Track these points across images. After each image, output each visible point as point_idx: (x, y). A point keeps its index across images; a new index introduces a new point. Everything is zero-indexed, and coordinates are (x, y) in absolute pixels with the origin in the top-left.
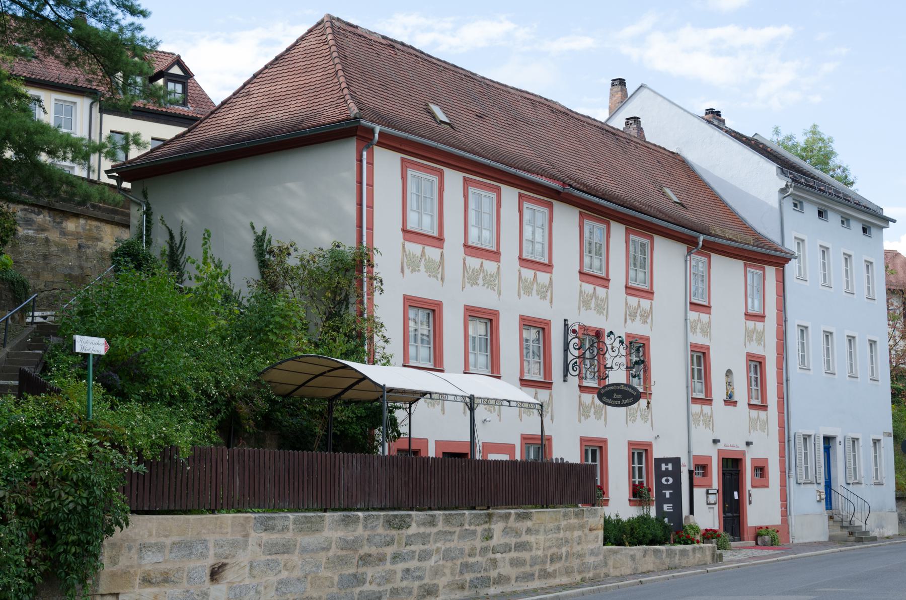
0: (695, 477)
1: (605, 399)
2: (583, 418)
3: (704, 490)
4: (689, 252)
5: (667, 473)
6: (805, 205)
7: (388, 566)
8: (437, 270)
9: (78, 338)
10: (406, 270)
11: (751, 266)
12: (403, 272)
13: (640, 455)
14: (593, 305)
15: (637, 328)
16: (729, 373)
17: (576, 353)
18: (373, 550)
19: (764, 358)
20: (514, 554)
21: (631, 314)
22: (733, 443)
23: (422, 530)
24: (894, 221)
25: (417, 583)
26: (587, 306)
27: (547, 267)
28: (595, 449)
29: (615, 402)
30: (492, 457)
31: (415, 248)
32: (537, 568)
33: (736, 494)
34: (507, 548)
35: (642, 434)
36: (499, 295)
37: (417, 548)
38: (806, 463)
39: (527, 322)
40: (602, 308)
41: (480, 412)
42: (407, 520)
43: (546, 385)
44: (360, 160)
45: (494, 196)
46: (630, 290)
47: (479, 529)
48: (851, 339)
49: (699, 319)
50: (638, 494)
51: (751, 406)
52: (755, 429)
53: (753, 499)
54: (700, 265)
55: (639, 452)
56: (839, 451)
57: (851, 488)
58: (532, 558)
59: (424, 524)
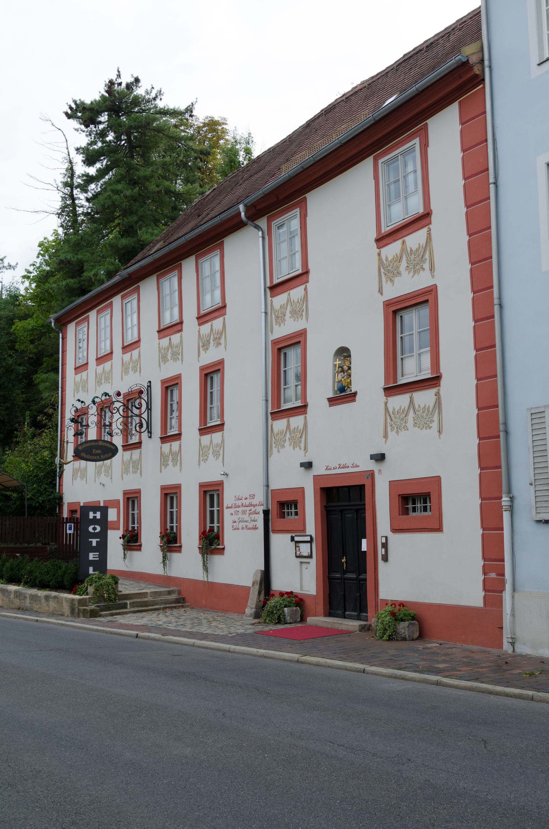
2: (163, 467)
5: (95, 521)
14: (169, 356)
16: (343, 353)
29: (95, 458)
36: (112, 385)
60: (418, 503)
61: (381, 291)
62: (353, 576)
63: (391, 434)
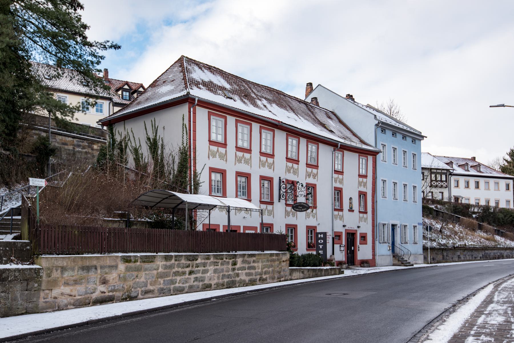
0: (335, 240)
1: (295, 208)
4: (334, 150)
5: (321, 238)
6: (387, 131)
7: (187, 276)
8: (223, 157)
9: (30, 179)
10: (211, 157)
11: (362, 156)
12: (209, 157)
13: (311, 231)
14: (292, 171)
15: (311, 181)
16: (351, 199)
17: (284, 190)
18: (180, 270)
19: (366, 193)
20: (247, 271)
21: (308, 175)
22: (352, 226)
23: (203, 261)
24: (426, 137)
25: (201, 283)
26: (289, 172)
27: (272, 156)
28: (292, 228)
30: (247, 232)
31: (214, 148)
32: (258, 277)
33: (353, 248)
34: (243, 269)
35: (312, 222)
37: (201, 268)
38: (384, 235)
39: (263, 178)
40: (296, 172)
41: (232, 212)
42: (196, 257)
43: (271, 203)
44: (190, 112)
45: (249, 127)
46: (308, 165)
47: (231, 261)
48: (405, 186)
50: (309, 246)
51: (360, 212)
52: (362, 221)
54: (339, 155)
55: (311, 230)
56: (398, 231)
57: (403, 245)
58: (256, 272)
59: (204, 259)
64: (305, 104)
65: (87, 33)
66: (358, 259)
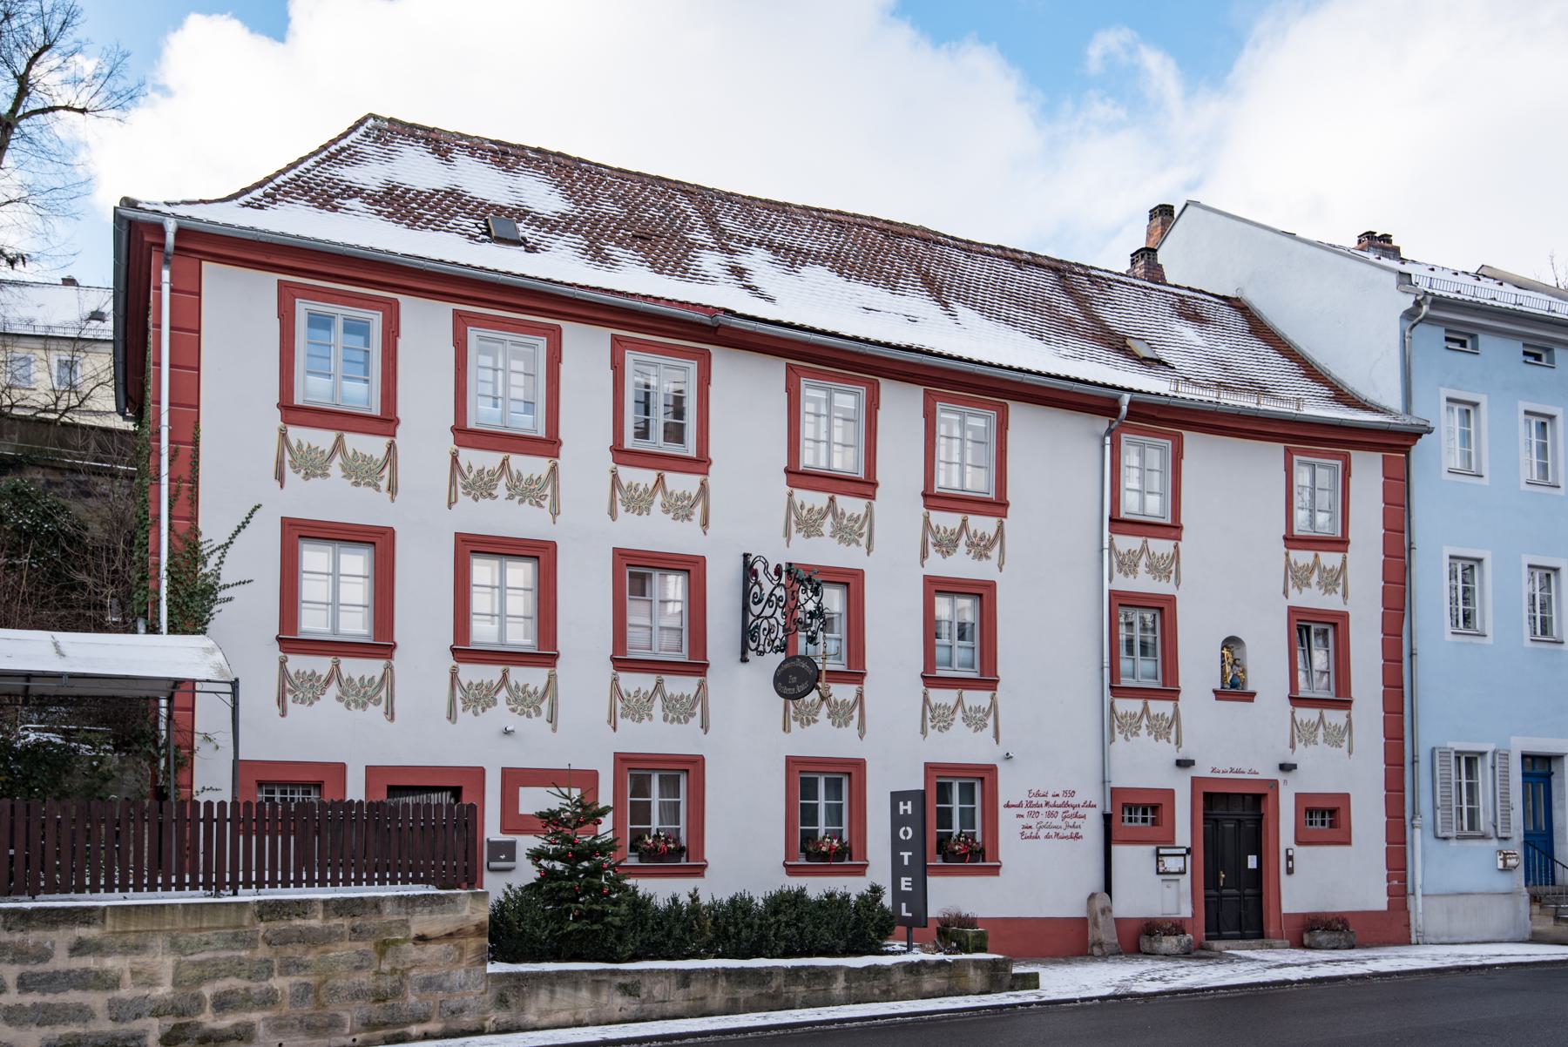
3: (1153, 848)
6: (1483, 339)
43: (696, 667)
45: (542, 343)
49: (1144, 549)
53: (1298, 864)
60: (1326, 818)
61: (1286, 593)
62: (1234, 891)
63: (1299, 746)
64: (1056, 270)
65: (768, 255)
66: (1287, 908)
